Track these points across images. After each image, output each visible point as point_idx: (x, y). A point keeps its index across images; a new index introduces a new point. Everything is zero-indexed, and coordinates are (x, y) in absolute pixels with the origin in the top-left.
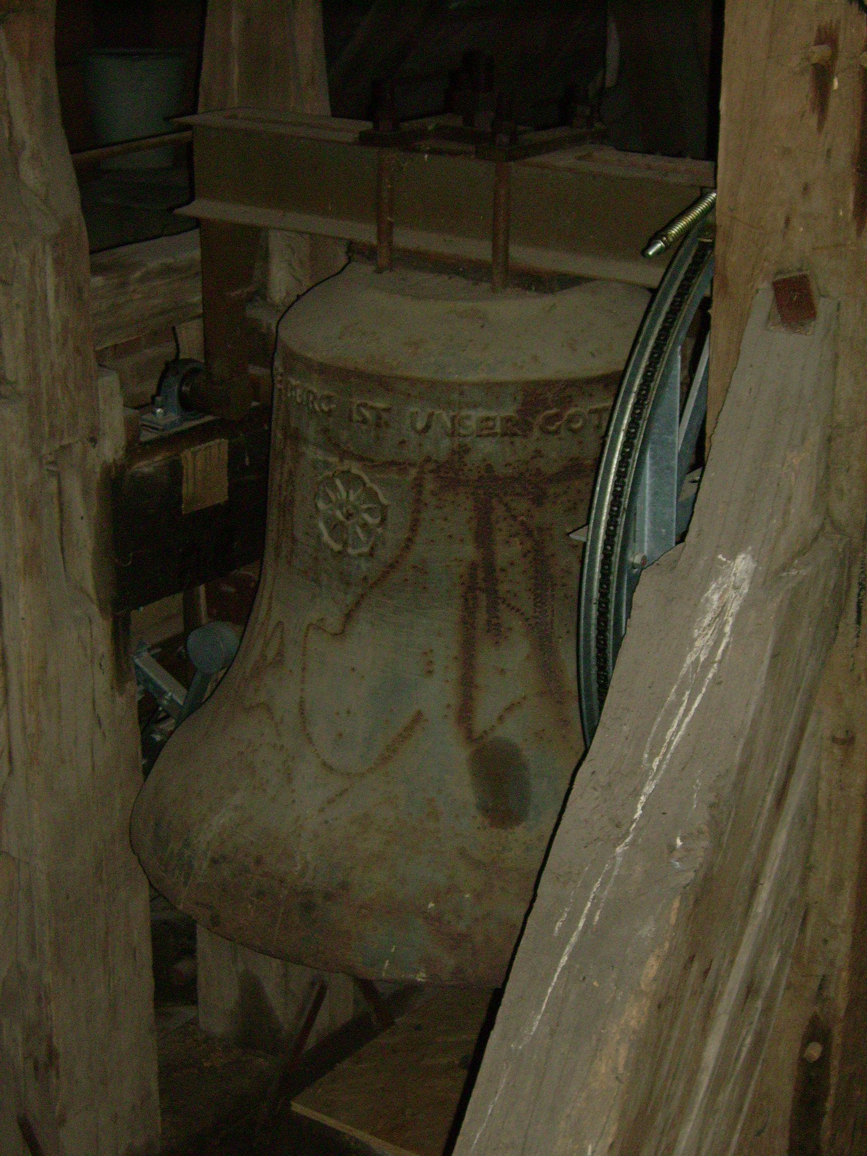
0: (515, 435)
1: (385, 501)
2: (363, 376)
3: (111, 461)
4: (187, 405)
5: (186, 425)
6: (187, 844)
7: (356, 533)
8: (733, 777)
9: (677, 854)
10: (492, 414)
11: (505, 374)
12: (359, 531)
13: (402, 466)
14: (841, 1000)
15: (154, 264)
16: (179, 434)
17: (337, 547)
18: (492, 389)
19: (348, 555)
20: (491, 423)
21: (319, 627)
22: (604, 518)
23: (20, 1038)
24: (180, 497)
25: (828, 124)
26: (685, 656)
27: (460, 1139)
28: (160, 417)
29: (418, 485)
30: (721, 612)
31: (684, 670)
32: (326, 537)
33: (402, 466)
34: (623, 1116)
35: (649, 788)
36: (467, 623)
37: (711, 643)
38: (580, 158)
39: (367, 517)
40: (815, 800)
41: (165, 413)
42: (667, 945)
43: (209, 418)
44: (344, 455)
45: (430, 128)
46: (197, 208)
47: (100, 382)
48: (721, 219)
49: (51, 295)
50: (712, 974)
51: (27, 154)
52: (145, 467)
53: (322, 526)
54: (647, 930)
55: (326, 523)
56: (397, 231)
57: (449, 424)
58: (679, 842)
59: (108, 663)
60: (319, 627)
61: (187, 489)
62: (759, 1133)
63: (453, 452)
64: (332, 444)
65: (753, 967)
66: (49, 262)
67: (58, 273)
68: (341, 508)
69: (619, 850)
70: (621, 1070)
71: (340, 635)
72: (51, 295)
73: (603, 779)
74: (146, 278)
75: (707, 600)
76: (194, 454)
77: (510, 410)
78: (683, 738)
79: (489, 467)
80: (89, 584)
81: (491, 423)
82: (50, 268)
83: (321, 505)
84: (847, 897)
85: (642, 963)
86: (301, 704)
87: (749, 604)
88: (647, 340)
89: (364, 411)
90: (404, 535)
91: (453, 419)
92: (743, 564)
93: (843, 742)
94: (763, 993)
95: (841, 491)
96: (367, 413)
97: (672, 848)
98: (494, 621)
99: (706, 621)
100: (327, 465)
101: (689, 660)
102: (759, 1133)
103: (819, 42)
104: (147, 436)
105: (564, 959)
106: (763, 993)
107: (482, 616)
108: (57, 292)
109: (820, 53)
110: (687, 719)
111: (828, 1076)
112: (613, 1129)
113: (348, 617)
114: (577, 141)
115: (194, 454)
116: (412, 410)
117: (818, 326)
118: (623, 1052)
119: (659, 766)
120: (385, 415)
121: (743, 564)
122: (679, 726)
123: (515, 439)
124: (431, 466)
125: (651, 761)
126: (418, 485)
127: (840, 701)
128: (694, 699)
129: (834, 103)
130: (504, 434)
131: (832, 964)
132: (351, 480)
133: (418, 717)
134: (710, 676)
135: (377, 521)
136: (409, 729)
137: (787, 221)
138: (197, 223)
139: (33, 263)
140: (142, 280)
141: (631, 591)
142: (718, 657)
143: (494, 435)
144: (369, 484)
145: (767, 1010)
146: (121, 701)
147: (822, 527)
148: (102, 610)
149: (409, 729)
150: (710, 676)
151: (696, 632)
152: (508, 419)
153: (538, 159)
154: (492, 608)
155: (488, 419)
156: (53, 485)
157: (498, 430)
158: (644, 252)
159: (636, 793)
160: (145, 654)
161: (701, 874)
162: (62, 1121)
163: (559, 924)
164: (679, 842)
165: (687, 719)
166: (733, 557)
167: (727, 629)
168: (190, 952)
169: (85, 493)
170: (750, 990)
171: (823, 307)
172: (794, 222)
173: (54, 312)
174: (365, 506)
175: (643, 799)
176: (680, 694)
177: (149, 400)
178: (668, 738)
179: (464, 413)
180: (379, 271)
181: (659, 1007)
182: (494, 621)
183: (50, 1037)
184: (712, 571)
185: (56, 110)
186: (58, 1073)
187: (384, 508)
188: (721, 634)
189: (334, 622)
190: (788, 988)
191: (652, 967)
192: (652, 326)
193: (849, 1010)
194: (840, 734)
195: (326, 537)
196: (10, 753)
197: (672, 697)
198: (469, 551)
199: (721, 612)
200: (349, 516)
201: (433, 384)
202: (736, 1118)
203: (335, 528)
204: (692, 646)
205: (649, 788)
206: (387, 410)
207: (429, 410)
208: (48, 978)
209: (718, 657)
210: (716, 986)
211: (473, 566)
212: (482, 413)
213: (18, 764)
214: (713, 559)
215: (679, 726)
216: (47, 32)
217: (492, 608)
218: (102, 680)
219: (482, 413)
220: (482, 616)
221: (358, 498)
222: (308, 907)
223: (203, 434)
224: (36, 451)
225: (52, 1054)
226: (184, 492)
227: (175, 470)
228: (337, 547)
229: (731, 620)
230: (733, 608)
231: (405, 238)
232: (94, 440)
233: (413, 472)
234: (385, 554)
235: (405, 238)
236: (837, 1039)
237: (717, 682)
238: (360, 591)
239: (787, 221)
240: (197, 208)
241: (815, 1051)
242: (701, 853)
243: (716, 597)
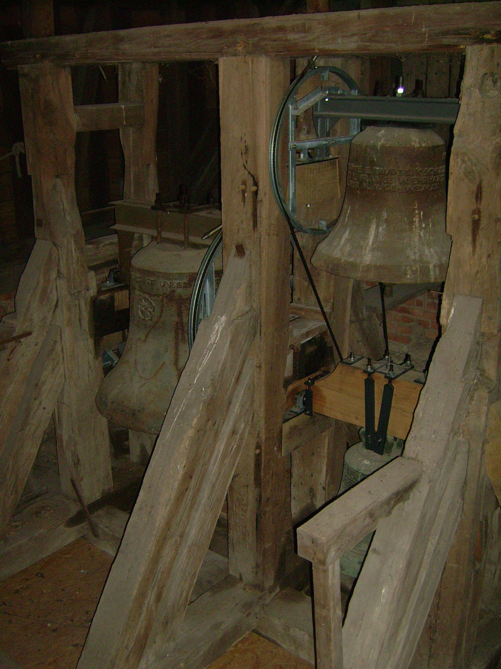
0: (187, 287)
1: (154, 305)
2: (148, 272)
3: (92, 296)
4: (116, 280)
5: (116, 286)
6: (106, 399)
7: (147, 314)
8: (219, 373)
9: (203, 392)
10: (181, 282)
11: (184, 271)
12: (148, 313)
13: (158, 296)
14: (263, 437)
15: (107, 242)
16: (113, 289)
17: (143, 318)
18: (181, 275)
19: (146, 320)
20: (180, 284)
21: (139, 339)
22: (194, 307)
23: (70, 456)
24: (114, 306)
25: (246, 206)
26: (208, 342)
27: (149, 465)
28: (108, 284)
29: (162, 300)
30: (218, 330)
31: (208, 346)
32: (141, 315)
33: (158, 296)
34: (188, 458)
35: (198, 376)
36: (176, 338)
37: (215, 339)
38: (208, 213)
39: (150, 309)
40: (253, 382)
41: (110, 283)
42: (199, 415)
43: (123, 284)
44: (144, 293)
45: (171, 205)
46: (117, 227)
47: (89, 274)
48: (223, 230)
49: (73, 250)
50: (217, 424)
51: (67, 212)
52: (103, 297)
53: (140, 312)
54: (195, 411)
55: (141, 311)
56: (163, 233)
57: (169, 284)
58: (204, 389)
59: (93, 351)
60: (139, 339)
61: (116, 304)
62: (247, 475)
63: (171, 292)
64: (141, 290)
65: (234, 426)
66: (73, 241)
67: (76, 244)
68: (144, 307)
69: (190, 391)
70: (187, 446)
71: (145, 341)
72: (73, 250)
73: (188, 374)
74: (105, 245)
75: (215, 328)
76: (118, 294)
77: (186, 281)
78: (207, 363)
79: (181, 296)
80: (87, 330)
81: (180, 284)
82: (73, 243)
83: (139, 306)
84: (263, 409)
85: (193, 420)
86: (135, 360)
87: (224, 329)
88: (206, 261)
89: (148, 281)
90: (159, 314)
91: (170, 283)
92: (224, 318)
93: (259, 367)
94: (239, 434)
95: (254, 300)
96: (149, 281)
97: (202, 390)
98: (183, 338)
99: (214, 333)
100: (140, 295)
101: (209, 343)
102: (247, 475)
103: (243, 184)
104: (103, 289)
105: (176, 419)
106: (239, 434)
107: (180, 336)
108: (75, 250)
109: (243, 187)
110: (208, 358)
111: (261, 459)
112: (185, 462)
113: (146, 336)
114: (207, 208)
115: (118, 294)
116: (160, 280)
117: (245, 258)
118: (188, 442)
119: (201, 370)
120: (153, 282)
121: (224, 318)
122: (206, 360)
123: (187, 288)
124: (165, 295)
125: (199, 369)
126: (162, 300)
127: (258, 356)
128: (210, 353)
129: (247, 200)
130: (184, 287)
131: (260, 427)
132: (146, 300)
133: (164, 363)
134: (214, 347)
135: (153, 310)
136: (162, 366)
137: (238, 230)
138: (116, 232)
139: (68, 242)
140: (103, 246)
141: (197, 325)
142: (216, 342)
143: (182, 287)
144: (150, 300)
145: (241, 439)
146: (97, 362)
147: (250, 310)
148: (91, 336)
149: (162, 366)
150: (214, 347)
151: (212, 336)
152: (185, 283)
153: (196, 213)
154: (183, 334)
155: (180, 283)
156: (77, 302)
157: (183, 286)
158: (202, 238)
159: (195, 378)
160: (111, 352)
161: (209, 397)
162: (82, 479)
163: (175, 410)
164: (204, 389)
165: (208, 358)
166: (221, 316)
167: (219, 335)
168: (127, 439)
169: (86, 304)
170: (234, 432)
171: (247, 253)
172: (240, 230)
173: (75, 255)
174: (149, 307)
175: (196, 378)
176: (207, 352)
177: (105, 280)
178: (203, 363)
179: (174, 281)
180: (158, 243)
181: (198, 431)
182: (183, 338)
183: (78, 455)
184: (217, 320)
185: (75, 200)
186: (80, 466)
187: (154, 307)
188: (217, 336)
189: (143, 338)
190: (249, 434)
191: (195, 421)
192: (207, 257)
193: (266, 440)
194: (258, 365)
195: (141, 315)
196: (65, 375)
197: (205, 352)
198: (176, 319)
199: (218, 330)
200: (146, 309)
201: (165, 273)
202: (233, 467)
203: (142, 312)
204: (210, 339)
205: (198, 376)
206: (154, 280)
207: (165, 281)
208: (77, 438)
209: (216, 342)
210: (218, 429)
211: (177, 323)
212: (178, 281)
213: (67, 378)
214: (217, 317)
215: (206, 360)
216: (72, 180)
217: (183, 334)
218: (91, 356)
219: (178, 281)
220: (180, 336)
221: (148, 304)
222: (134, 414)
223: (121, 289)
224: (69, 292)
225: (79, 460)
226: (115, 305)
227: (112, 299)
228: (143, 318)
229: (220, 333)
230: (220, 330)
231: (165, 234)
232: (88, 290)
233: (161, 297)
234: (155, 319)
235: (165, 234)
236: (263, 448)
237: (215, 348)
238: (149, 329)
239: (238, 230)
240: (117, 227)
241: (258, 451)
242: (209, 392)
243: (217, 327)
